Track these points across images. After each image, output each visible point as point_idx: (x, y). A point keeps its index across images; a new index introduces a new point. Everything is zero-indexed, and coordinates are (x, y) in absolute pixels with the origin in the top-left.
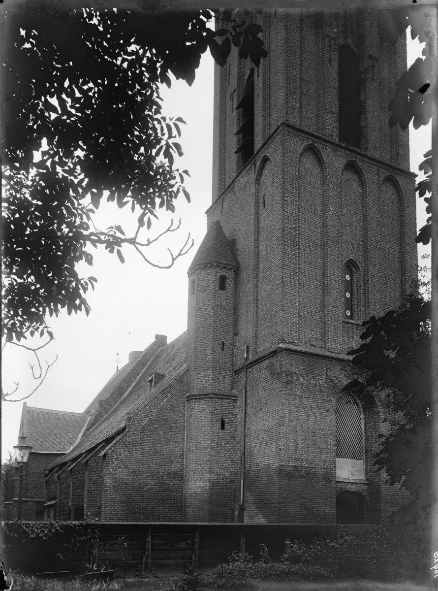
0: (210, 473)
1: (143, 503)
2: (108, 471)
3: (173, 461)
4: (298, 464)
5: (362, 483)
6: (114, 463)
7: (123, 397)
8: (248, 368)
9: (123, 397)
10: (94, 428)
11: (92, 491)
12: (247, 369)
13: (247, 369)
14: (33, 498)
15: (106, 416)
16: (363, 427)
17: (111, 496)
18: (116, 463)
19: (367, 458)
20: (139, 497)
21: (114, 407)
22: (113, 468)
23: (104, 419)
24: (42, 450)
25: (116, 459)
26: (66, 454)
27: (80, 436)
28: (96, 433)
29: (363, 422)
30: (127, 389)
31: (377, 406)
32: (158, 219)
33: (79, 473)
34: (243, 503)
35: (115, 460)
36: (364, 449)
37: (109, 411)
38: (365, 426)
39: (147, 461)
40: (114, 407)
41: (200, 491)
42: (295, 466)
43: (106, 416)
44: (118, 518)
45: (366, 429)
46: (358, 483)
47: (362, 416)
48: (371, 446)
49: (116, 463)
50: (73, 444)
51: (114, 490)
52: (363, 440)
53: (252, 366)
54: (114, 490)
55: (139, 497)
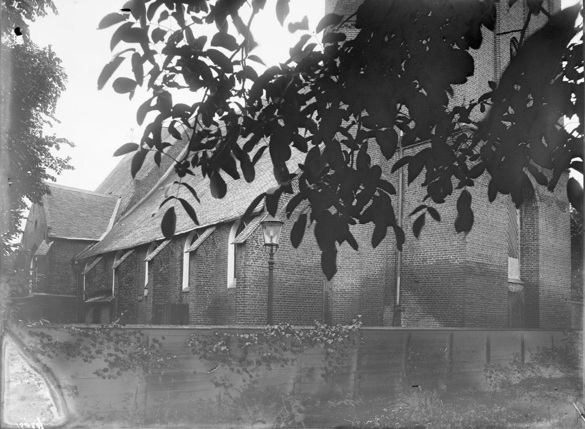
0: (361, 268)
1: (284, 301)
2: (248, 263)
3: (314, 253)
4: (480, 260)
5: (520, 284)
6: (254, 253)
7: (162, 179)
8: (405, 149)
9: (162, 179)
10: (130, 212)
11: (201, 286)
12: (403, 150)
13: (403, 150)
14: (59, 293)
15: (142, 199)
16: (518, 222)
17: (252, 292)
18: (256, 253)
19: (522, 256)
20: (280, 294)
21: (152, 190)
22: (253, 259)
23: (140, 202)
24: (69, 235)
25: (257, 247)
26: (98, 241)
27: (112, 221)
28: (140, 218)
29: (518, 217)
30: (167, 169)
31: (536, 201)
32: (57, 13)
33: (161, 264)
34: (400, 303)
35: (255, 249)
36: (519, 246)
37: (146, 193)
38: (521, 221)
39: (288, 251)
40: (152, 190)
41: (348, 288)
42: (478, 263)
43: (142, 199)
44: (259, 319)
45: (521, 225)
46: (517, 284)
47: (518, 211)
48: (527, 244)
49: (256, 253)
50: (105, 230)
51: (255, 286)
52: (519, 237)
53: (413, 147)
54: (255, 286)
55: (280, 294)
